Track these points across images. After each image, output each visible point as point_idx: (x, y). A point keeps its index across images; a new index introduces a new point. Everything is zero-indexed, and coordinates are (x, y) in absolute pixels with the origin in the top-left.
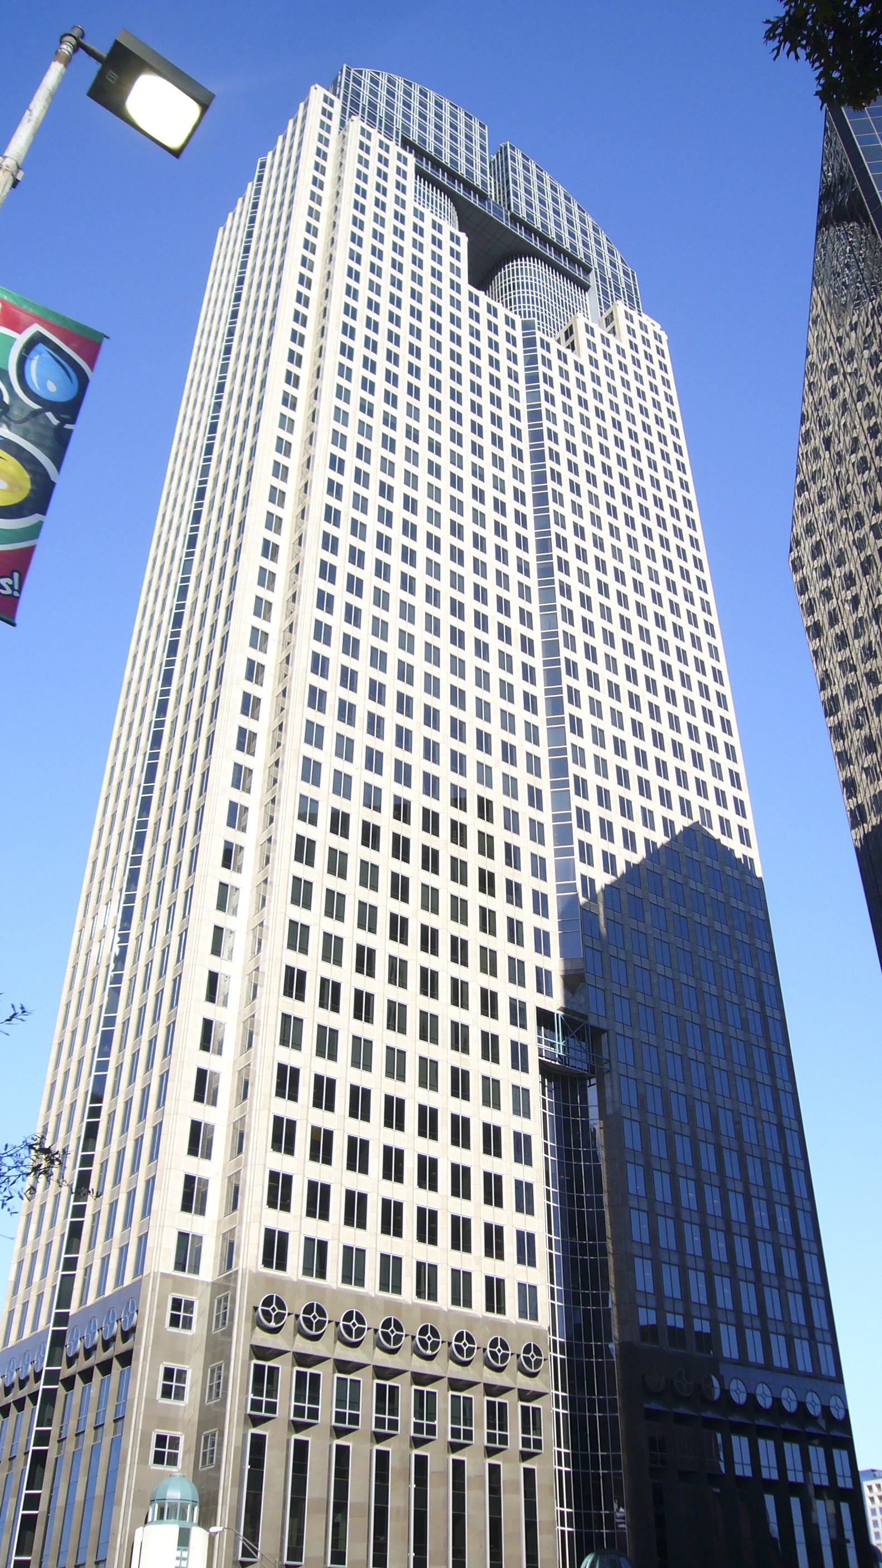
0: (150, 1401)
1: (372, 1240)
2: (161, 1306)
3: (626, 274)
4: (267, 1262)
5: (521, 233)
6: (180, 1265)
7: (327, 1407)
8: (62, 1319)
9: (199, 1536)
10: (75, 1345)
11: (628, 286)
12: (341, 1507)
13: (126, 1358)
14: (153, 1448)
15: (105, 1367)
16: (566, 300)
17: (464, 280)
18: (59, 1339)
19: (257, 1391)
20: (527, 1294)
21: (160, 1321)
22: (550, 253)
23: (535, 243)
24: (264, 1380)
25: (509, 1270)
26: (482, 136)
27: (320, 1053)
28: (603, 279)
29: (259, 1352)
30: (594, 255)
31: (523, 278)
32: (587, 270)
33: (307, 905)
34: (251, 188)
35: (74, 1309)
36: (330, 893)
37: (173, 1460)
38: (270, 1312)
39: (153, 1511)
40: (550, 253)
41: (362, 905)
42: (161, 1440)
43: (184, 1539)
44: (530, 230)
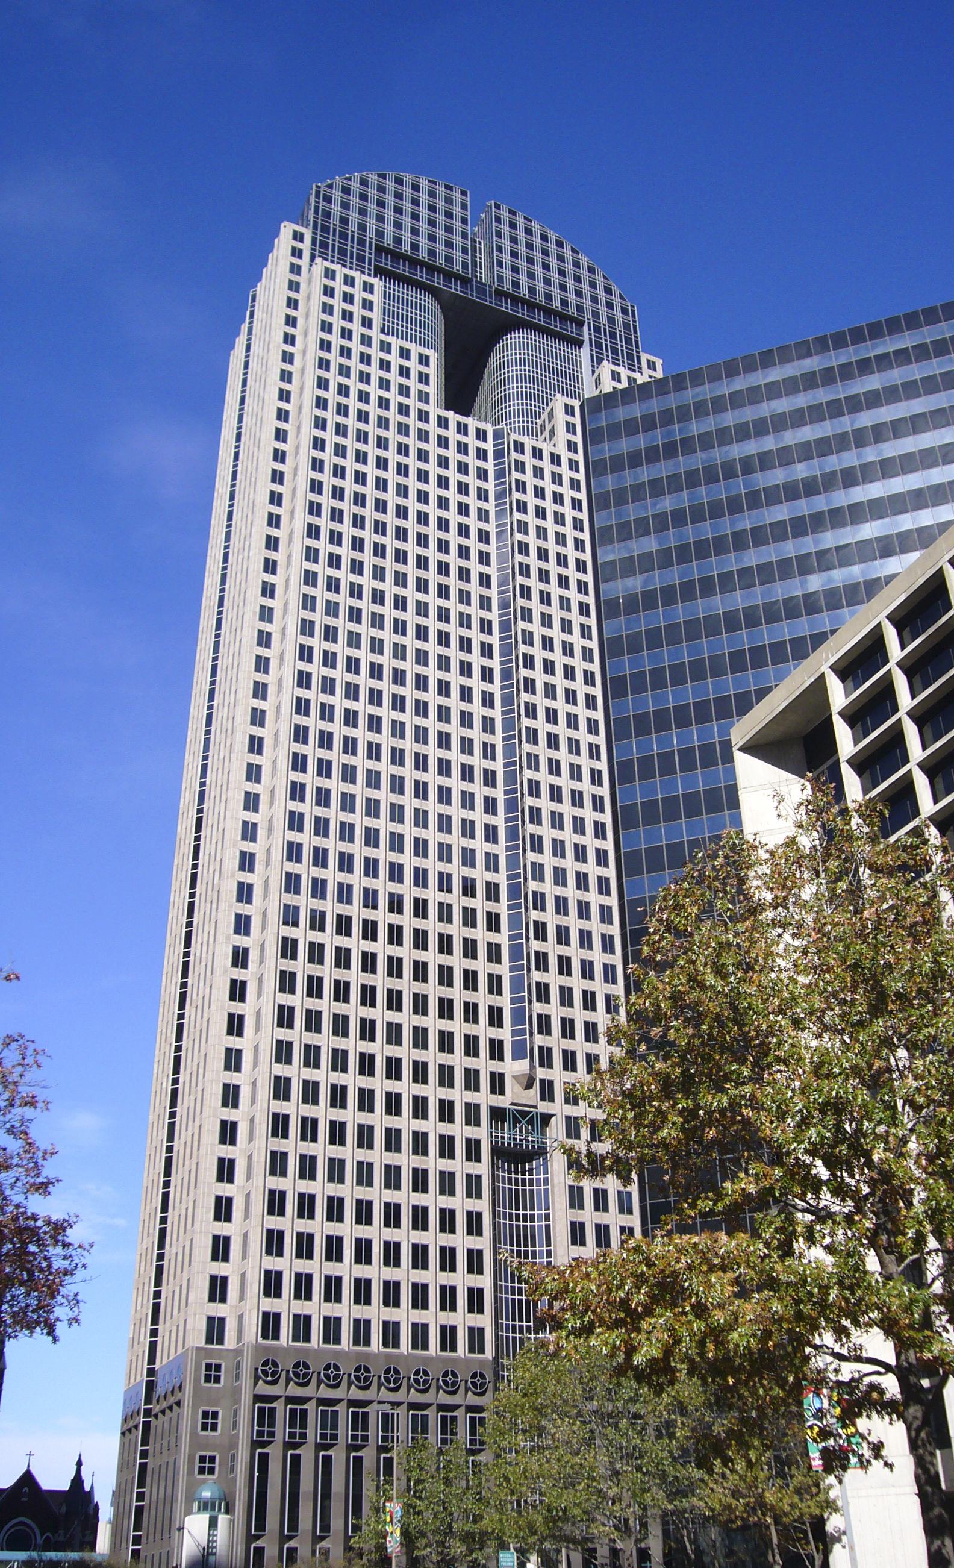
0: (193, 1434)
1: (346, 1310)
2: (197, 1370)
3: (624, 311)
4: (265, 1336)
5: (506, 307)
6: (209, 1340)
7: (312, 1432)
8: (151, 1372)
9: (223, 1519)
10: (159, 1391)
11: (626, 326)
12: (327, 1495)
13: (178, 1404)
14: (197, 1465)
15: (171, 1408)
16: (559, 365)
17: (434, 410)
18: (150, 1386)
19: (261, 1424)
20: (476, 1336)
21: (197, 1380)
22: (539, 319)
23: (522, 313)
24: (265, 1416)
25: (461, 1319)
26: (464, 207)
27: (561, 973)
28: (597, 330)
29: (257, 1398)
30: (587, 304)
31: (513, 354)
32: (580, 324)
33: (559, 774)
34: (244, 328)
35: (157, 1366)
36: (552, 786)
37: (211, 1471)
38: (268, 1370)
39: (195, 1505)
40: (539, 319)
41: (574, 818)
42: (202, 1459)
43: (213, 1523)
44: (516, 300)
